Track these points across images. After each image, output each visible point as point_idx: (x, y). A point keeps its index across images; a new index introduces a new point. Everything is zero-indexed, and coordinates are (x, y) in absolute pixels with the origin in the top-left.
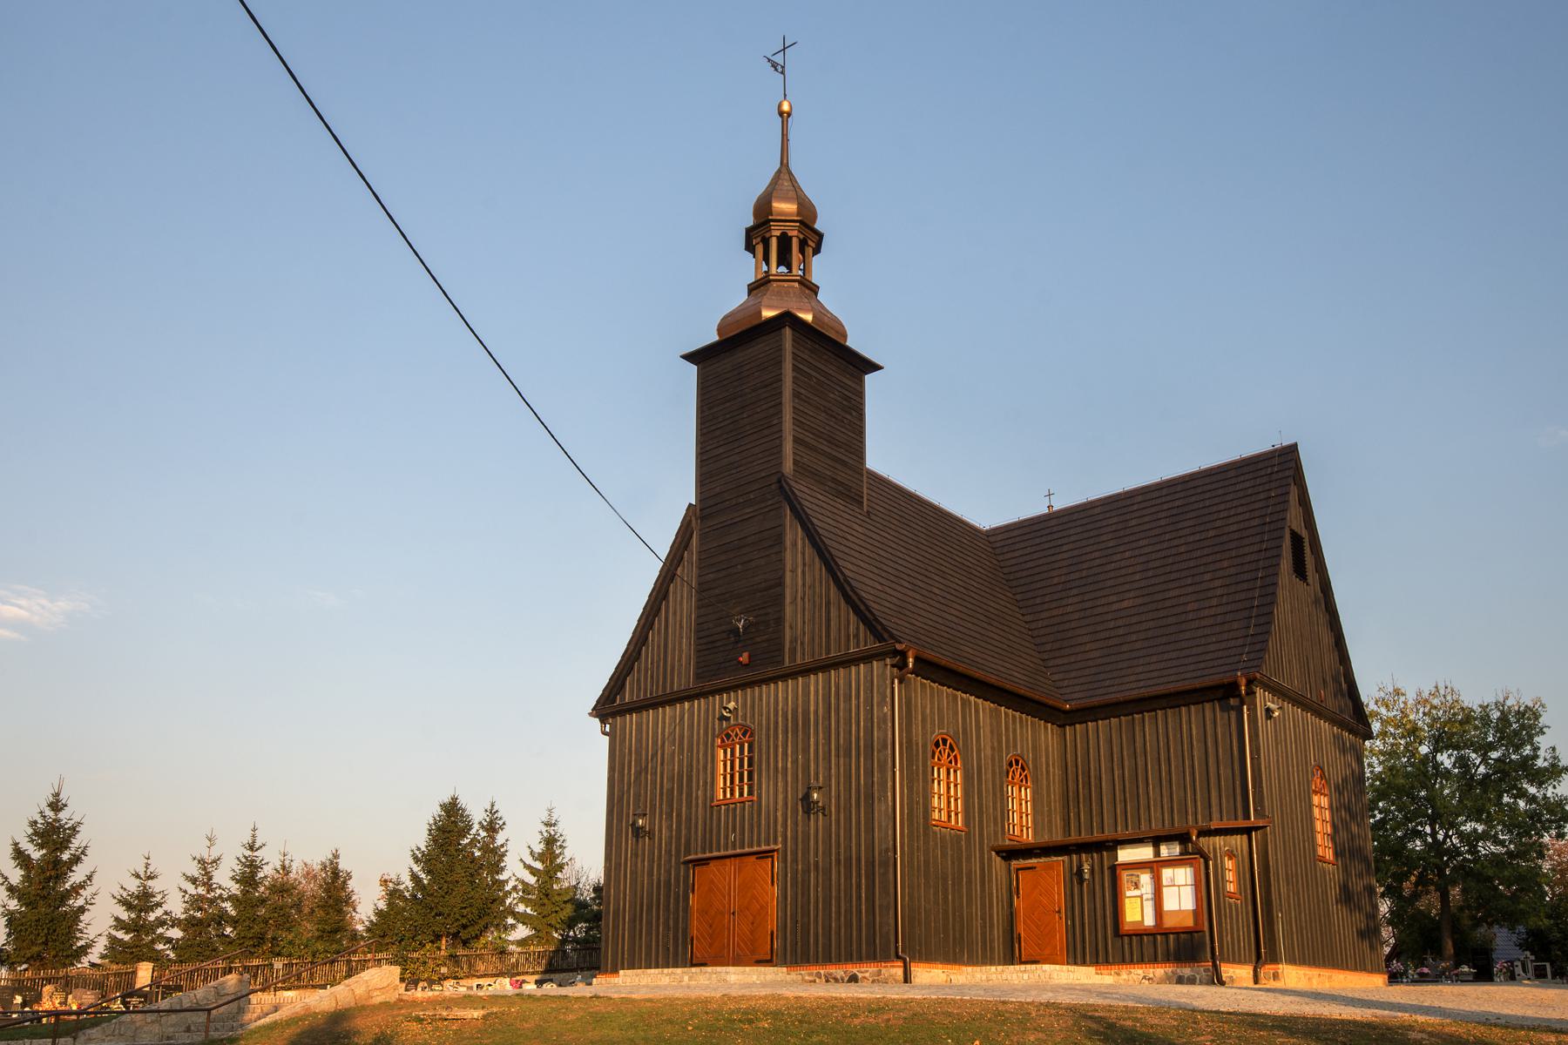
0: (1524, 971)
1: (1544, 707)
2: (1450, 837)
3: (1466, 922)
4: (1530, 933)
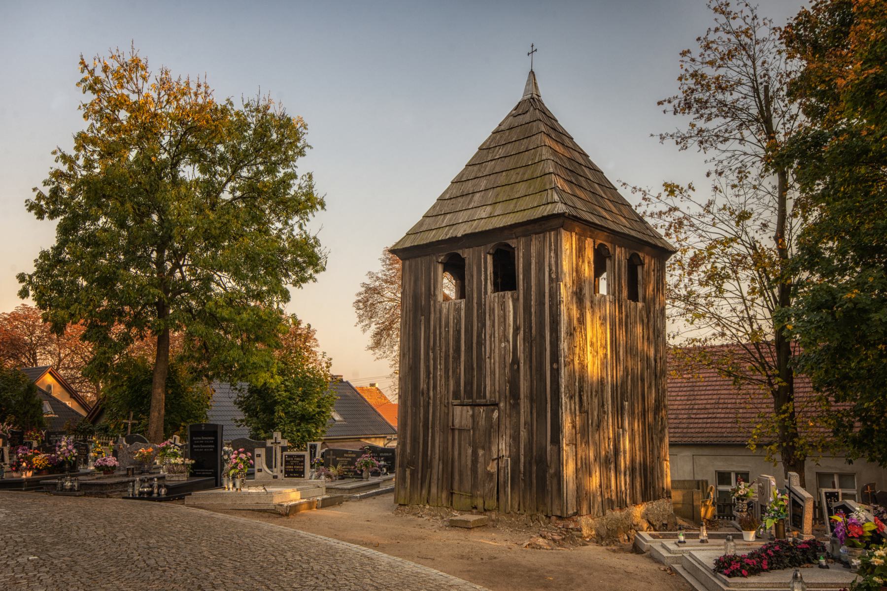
0: (270, 466)
1: (305, 128)
2: (180, 267)
3: (184, 372)
4: (253, 391)
